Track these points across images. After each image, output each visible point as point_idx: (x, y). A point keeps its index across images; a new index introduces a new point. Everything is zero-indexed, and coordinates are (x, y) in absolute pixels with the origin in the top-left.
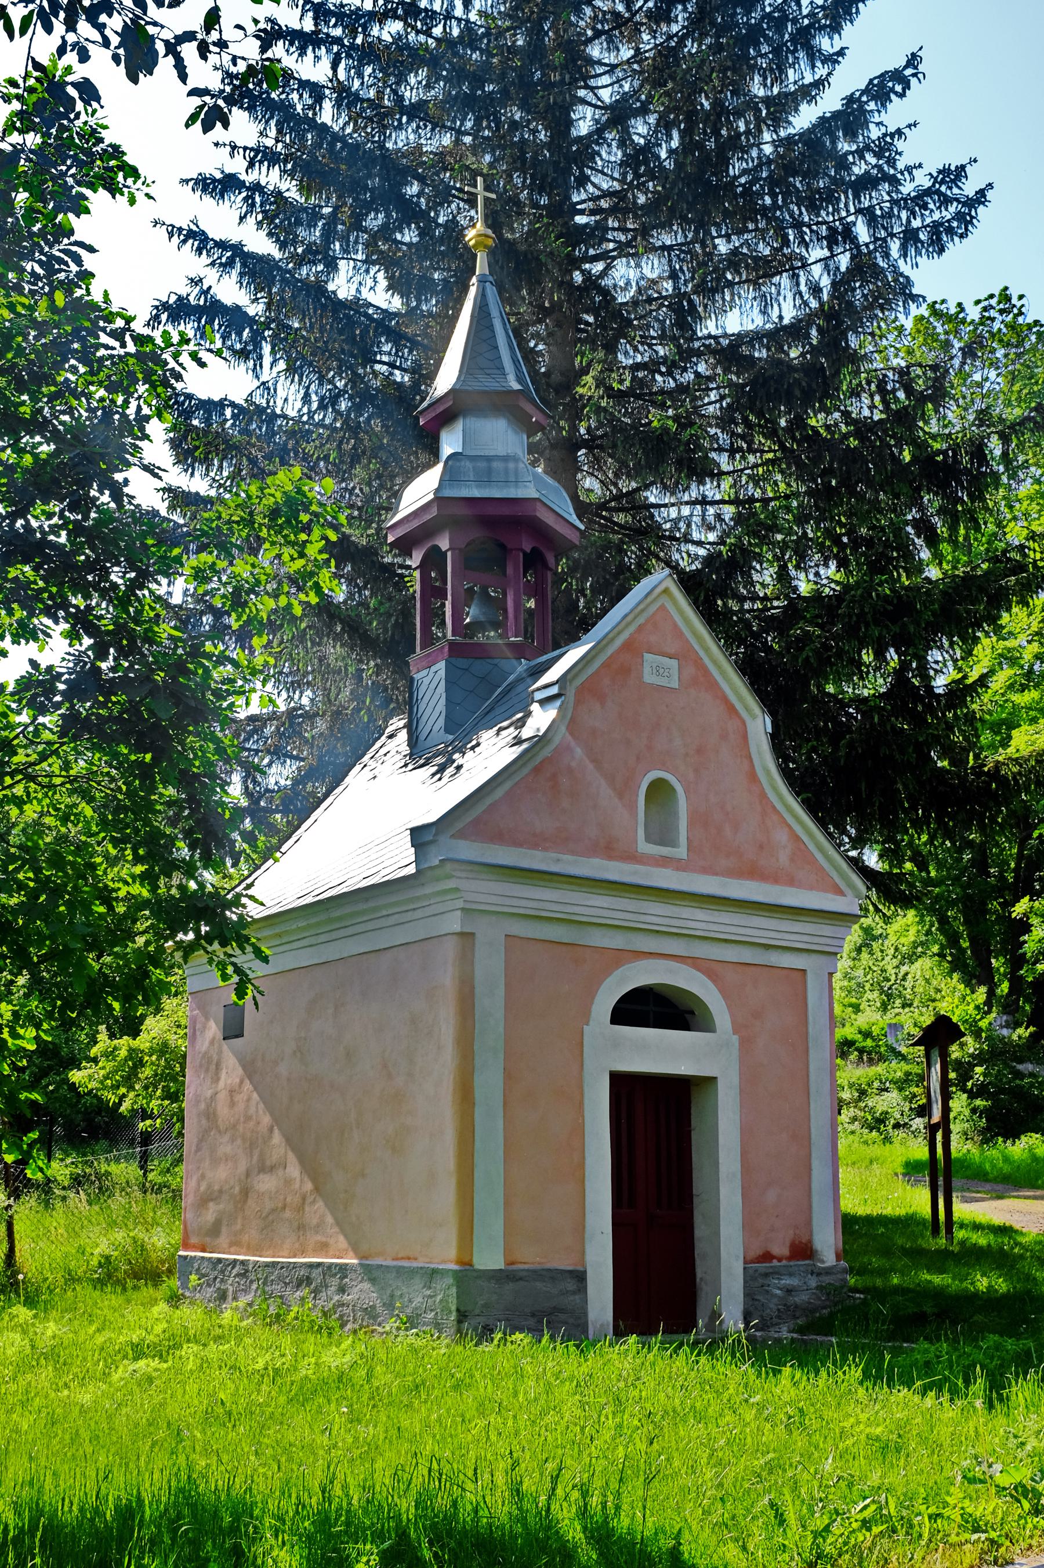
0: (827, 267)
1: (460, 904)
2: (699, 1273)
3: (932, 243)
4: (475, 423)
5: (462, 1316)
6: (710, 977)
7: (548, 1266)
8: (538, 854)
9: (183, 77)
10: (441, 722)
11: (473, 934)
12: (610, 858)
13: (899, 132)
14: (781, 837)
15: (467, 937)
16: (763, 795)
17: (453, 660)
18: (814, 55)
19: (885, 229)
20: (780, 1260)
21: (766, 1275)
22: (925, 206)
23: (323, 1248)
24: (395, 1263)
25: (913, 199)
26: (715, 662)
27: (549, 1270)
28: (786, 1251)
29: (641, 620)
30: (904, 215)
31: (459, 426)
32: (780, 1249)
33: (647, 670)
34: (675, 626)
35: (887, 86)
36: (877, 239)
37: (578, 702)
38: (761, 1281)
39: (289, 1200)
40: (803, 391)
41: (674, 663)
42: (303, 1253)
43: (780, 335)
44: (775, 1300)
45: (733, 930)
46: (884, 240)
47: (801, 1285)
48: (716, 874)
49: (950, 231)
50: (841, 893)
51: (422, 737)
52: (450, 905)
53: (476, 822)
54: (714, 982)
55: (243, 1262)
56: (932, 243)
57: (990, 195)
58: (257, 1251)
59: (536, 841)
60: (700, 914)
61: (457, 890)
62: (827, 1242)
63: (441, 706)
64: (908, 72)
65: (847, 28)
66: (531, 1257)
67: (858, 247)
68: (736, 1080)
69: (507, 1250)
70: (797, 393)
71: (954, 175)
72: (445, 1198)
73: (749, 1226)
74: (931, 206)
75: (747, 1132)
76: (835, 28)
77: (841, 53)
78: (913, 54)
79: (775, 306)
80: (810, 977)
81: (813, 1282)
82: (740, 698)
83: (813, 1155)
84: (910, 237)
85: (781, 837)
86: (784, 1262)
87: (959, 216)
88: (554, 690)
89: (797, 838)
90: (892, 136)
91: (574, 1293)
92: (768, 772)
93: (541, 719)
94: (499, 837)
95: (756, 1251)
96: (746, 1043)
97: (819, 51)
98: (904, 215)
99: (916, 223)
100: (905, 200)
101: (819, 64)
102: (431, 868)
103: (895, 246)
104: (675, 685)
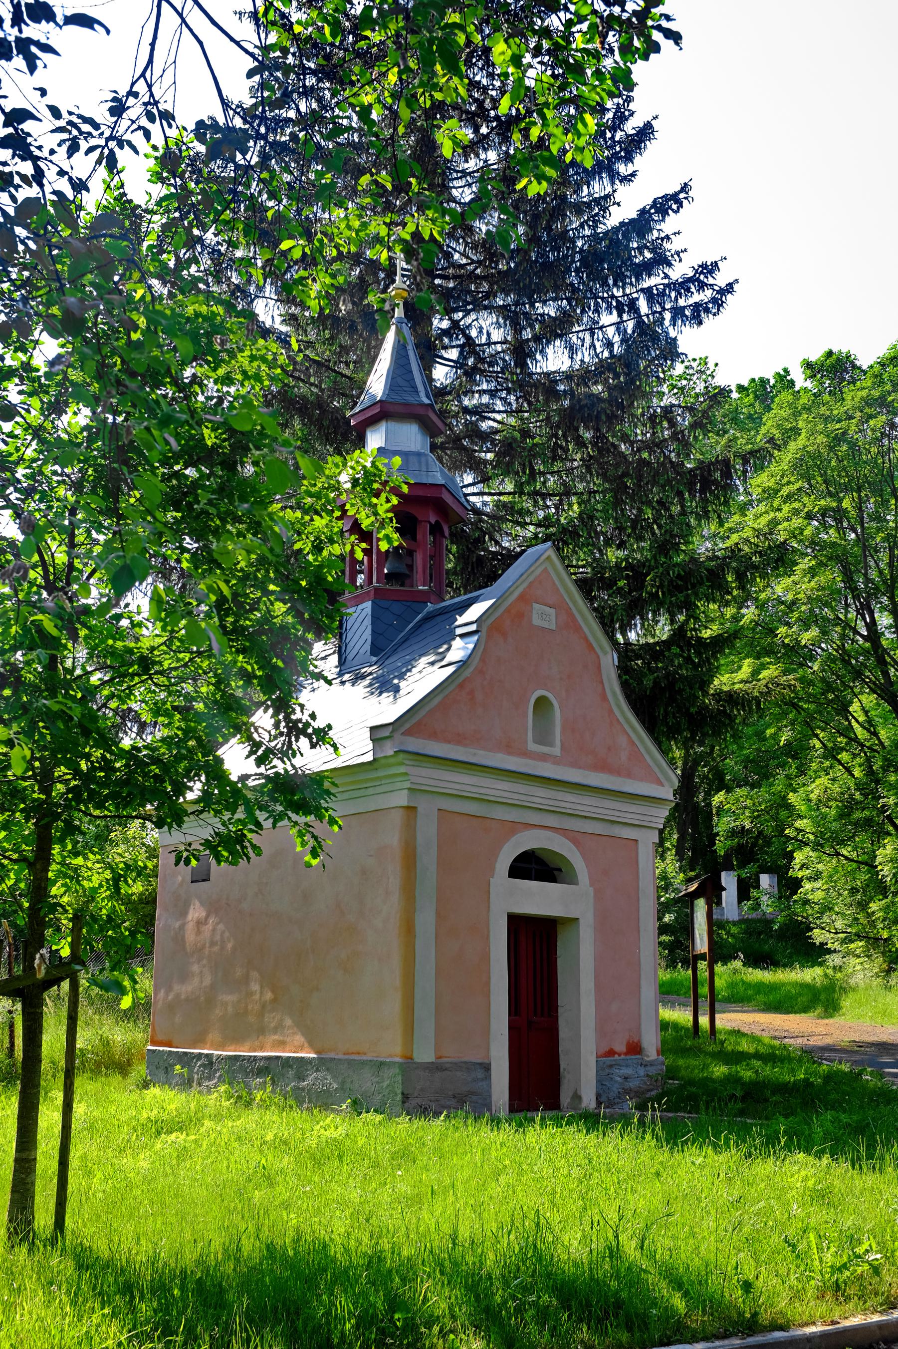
0: (618, 329)
1: (407, 785)
2: (563, 1064)
3: (694, 318)
4: (394, 426)
5: (406, 1098)
6: (574, 843)
7: (466, 1059)
8: (461, 749)
9: (137, 152)
10: (368, 647)
11: (415, 808)
12: (509, 754)
13: (668, 238)
14: (622, 741)
15: (411, 809)
16: (611, 711)
17: (377, 601)
18: (614, 176)
19: (660, 304)
20: (620, 1055)
21: (611, 1066)
22: (688, 290)
23: (281, 1044)
24: (346, 1057)
25: (680, 284)
26: (580, 612)
27: (466, 1063)
28: (624, 1050)
29: (531, 578)
30: (673, 294)
31: (383, 427)
32: (620, 1047)
33: (535, 616)
34: (554, 584)
35: (667, 204)
36: (654, 313)
37: (489, 636)
38: (607, 1071)
39: (250, 1007)
40: (607, 415)
41: (552, 611)
42: (262, 1049)
43: (584, 376)
44: (616, 1085)
45: (589, 809)
46: (660, 313)
47: (634, 1074)
48: (580, 768)
49: (707, 310)
50: (662, 784)
51: (350, 658)
52: (399, 785)
53: (419, 723)
54: (577, 847)
55: (207, 1055)
56: (694, 318)
57: (736, 287)
58: (222, 1047)
59: (459, 739)
60: (570, 798)
61: (406, 774)
62: (651, 1042)
63: (368, 635)
64: (682, 196)
65: (638, 159)
66: (453, 1053)
67: (640, 316)
68: (591, 921)
69: (437, 1048)
70: (604, 418)
71: (709, 269)
72: (393, 1006)
73: (601, 1031)
74: (693, 290)
75: (599, 959)
76: (629, 159)
77: (633, 174)
78: (685, 184)
79: (579, 354)
80: (640, 845)
81: (642, 1071)
82: (596, 639)
83: (642, 976)
84: (678, 313)
85: (622, 741)
86: (623, 1057)
87: (714, 300)
88: (473, 627)
89: (633, 743)
90: (662, 239)
91: (482, 1080)
92: (614, 694)
93: (459, 650)
94: (433, 735)
95: (605, 1048)
96: (599, 895)
97: (618, 173)
98: (673, 294)
99: (682, 302)
100: (674, 284)
101: (617, 182)
102: (386, 757)
103: (668, 316)
104: (553, 627)
